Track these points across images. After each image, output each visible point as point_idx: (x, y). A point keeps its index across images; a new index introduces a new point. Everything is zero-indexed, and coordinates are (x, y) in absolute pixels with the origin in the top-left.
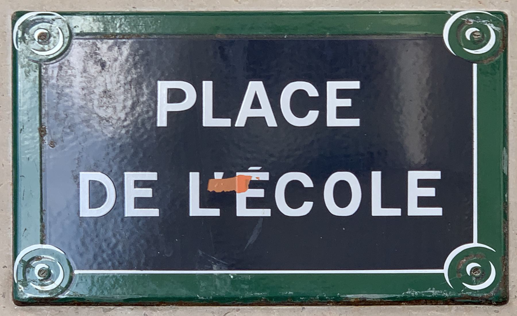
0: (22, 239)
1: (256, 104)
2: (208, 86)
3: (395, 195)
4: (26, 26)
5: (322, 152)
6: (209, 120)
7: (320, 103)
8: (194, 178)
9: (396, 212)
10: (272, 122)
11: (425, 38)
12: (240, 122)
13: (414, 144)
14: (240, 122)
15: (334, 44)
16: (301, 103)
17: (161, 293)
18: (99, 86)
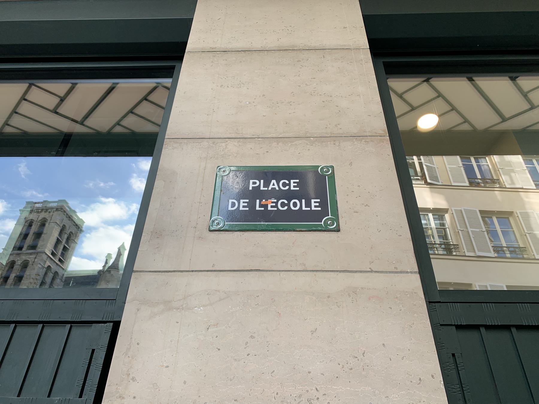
0: (213, 215)
1: (274, 185)
2: (262, 181)
3: (308, 204)
4: (220, 169)
5: (289, 195)
6: (262, 188)
7: (289, 185)
8: (258, 201)
9: (309, 209)
10: (277, 189)
11: (314, 171)
12: (270, 189)
13: (312, 193)
14: (270, 189)
15: (293, 172)
16: (284, 185)
17: (248, 228)
18: (235, 183)
